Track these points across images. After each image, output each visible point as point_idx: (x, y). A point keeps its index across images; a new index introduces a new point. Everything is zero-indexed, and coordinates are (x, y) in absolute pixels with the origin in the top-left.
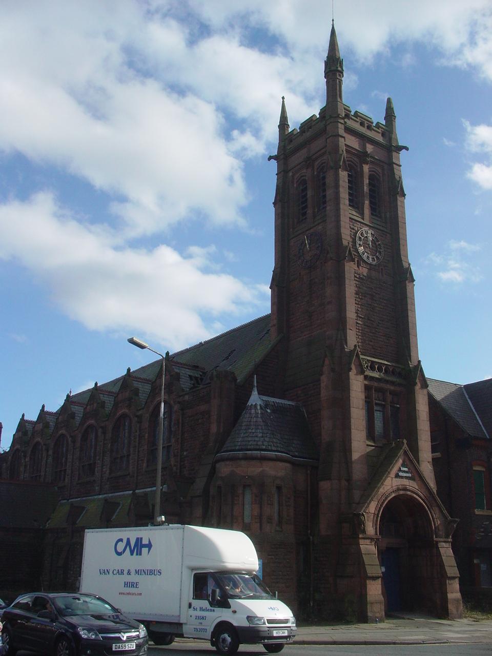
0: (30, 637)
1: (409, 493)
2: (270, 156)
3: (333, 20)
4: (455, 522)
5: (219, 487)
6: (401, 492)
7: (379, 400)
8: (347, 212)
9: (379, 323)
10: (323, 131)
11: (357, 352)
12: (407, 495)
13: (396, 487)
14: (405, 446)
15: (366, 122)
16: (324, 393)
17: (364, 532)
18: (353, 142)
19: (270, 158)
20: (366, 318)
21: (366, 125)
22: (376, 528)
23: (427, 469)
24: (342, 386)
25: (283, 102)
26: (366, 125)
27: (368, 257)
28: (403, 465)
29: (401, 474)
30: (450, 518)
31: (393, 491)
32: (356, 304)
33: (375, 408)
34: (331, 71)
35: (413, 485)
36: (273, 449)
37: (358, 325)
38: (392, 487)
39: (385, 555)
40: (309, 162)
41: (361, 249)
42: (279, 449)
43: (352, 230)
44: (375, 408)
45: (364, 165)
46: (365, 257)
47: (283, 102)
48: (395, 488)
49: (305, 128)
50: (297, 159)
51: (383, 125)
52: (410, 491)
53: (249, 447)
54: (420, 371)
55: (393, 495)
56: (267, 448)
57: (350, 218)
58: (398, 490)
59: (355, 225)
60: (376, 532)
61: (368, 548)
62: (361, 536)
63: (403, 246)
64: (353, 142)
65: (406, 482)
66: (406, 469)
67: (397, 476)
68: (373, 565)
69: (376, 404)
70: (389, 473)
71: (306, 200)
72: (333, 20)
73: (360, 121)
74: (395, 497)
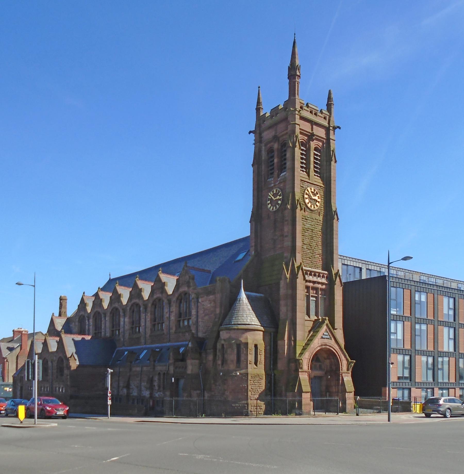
0: (202, 384)
1: (328, 347)
2: (250, 131)
3: (295, 34)
4: (352, 362)
5: (223, 345)
6: (324, 347)
7: (314, 294)
8: (300, 174)
9: (315, 246)
10: (285, 119)
11: (300, 202)
12: (327, 348)
13: (321, 344)
14: (327, 322)
15: (314, 110)
16: (282, 291)
17: (302, 368)
18: (307, 127)
19: (250, 132)
20: (308, 244)
21: (314, 113)
22: (309, 366)
23: (339, 334)
24: (293, 286)
26: (314, 113)
27: (311, 206)
28: (326, 331)
29: (324, 337)
30: (350, 360)
31: (319, 346)
32: (302, 235)
33: (311, 298)
34: (292, 75)
35: (332, 342)
36: (253, 324)
37: (303, 249)
38: (318, 344)
39: (312, 380)
40: (276, 138)
41: (307, 201)
42: (256, 324)
43: (302, 188)
44: (311, 298)
45: (311, 142)
48: (320, 344)
49: (273, 114)
50: (267, 135)
51: (320, 145)
52: (328, 346)
53: (239, 323)
54: (339, 276)
55: (319, 348)
56: (250, 324)
57: (301, 180)
58: (322, 345)
59: (304, 184)
60: (308, 368)
61: (304, 377)
62: (300, 370)
63: (333, 196)
64: (307, 127)
65: (326, 341)
66: (327, 334)
67: (322, 338)
68: (306, 386)
69: (312, 296)
70: (317, 336)
71: (273, 164)
72: (295, 34)
73: (310, 110)
74: (320, 349)
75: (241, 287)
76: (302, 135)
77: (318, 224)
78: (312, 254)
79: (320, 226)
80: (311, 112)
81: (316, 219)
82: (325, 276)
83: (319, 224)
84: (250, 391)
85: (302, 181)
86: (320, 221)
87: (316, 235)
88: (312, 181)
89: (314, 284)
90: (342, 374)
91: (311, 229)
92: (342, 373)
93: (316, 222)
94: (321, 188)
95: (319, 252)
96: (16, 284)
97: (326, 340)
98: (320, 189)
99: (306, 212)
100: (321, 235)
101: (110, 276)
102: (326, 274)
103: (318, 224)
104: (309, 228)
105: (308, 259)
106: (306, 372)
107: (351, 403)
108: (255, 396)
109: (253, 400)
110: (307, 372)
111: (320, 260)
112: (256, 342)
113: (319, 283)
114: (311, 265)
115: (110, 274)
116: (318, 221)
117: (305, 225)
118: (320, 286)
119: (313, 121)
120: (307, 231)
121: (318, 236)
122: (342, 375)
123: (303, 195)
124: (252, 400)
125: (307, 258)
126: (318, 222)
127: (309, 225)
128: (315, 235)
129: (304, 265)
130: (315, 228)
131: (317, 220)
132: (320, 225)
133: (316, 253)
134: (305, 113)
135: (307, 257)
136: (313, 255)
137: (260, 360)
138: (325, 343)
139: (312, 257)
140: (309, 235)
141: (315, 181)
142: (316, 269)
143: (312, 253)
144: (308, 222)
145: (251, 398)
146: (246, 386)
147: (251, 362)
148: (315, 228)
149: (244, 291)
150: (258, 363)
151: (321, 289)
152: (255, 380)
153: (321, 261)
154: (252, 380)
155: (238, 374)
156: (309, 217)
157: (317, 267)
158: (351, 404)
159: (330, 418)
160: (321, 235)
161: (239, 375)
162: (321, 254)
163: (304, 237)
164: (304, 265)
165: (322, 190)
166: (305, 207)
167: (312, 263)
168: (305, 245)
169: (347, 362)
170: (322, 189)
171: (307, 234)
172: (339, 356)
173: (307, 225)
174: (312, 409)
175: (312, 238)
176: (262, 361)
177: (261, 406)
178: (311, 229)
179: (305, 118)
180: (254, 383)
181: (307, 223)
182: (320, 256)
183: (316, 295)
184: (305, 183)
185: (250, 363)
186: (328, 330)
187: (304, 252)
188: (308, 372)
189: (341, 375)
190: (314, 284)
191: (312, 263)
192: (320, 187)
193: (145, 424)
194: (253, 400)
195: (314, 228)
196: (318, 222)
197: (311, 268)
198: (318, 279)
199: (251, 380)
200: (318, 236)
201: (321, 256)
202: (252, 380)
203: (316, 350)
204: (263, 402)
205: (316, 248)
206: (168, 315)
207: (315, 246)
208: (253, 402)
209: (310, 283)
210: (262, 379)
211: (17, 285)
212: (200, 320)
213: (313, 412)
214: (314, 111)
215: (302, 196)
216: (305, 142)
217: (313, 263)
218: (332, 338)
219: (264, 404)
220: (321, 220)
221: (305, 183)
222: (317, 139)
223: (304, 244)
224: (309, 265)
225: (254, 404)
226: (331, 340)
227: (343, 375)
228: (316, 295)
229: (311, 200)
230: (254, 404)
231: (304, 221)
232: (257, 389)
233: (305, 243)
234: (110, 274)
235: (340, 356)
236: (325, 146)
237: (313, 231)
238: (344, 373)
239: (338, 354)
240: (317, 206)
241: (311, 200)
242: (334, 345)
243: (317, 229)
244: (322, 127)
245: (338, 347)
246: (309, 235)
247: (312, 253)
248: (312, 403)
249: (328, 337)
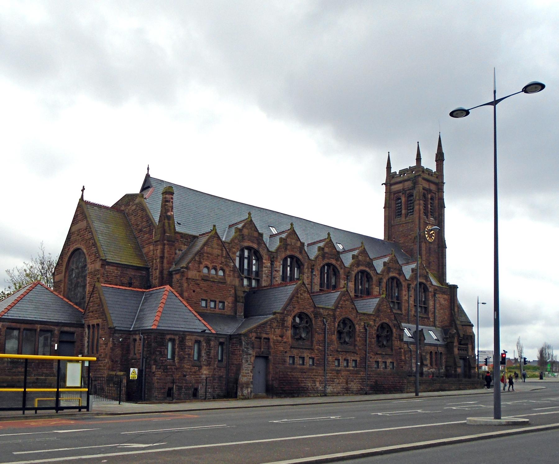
25: (418, 145)
27: (429, 239)
47: (418, 145)
101: (148, 170)
115: (148, 168)
206: (406, 298)
212: (437, 311)
234: (148, 168)
240: (433, 239)
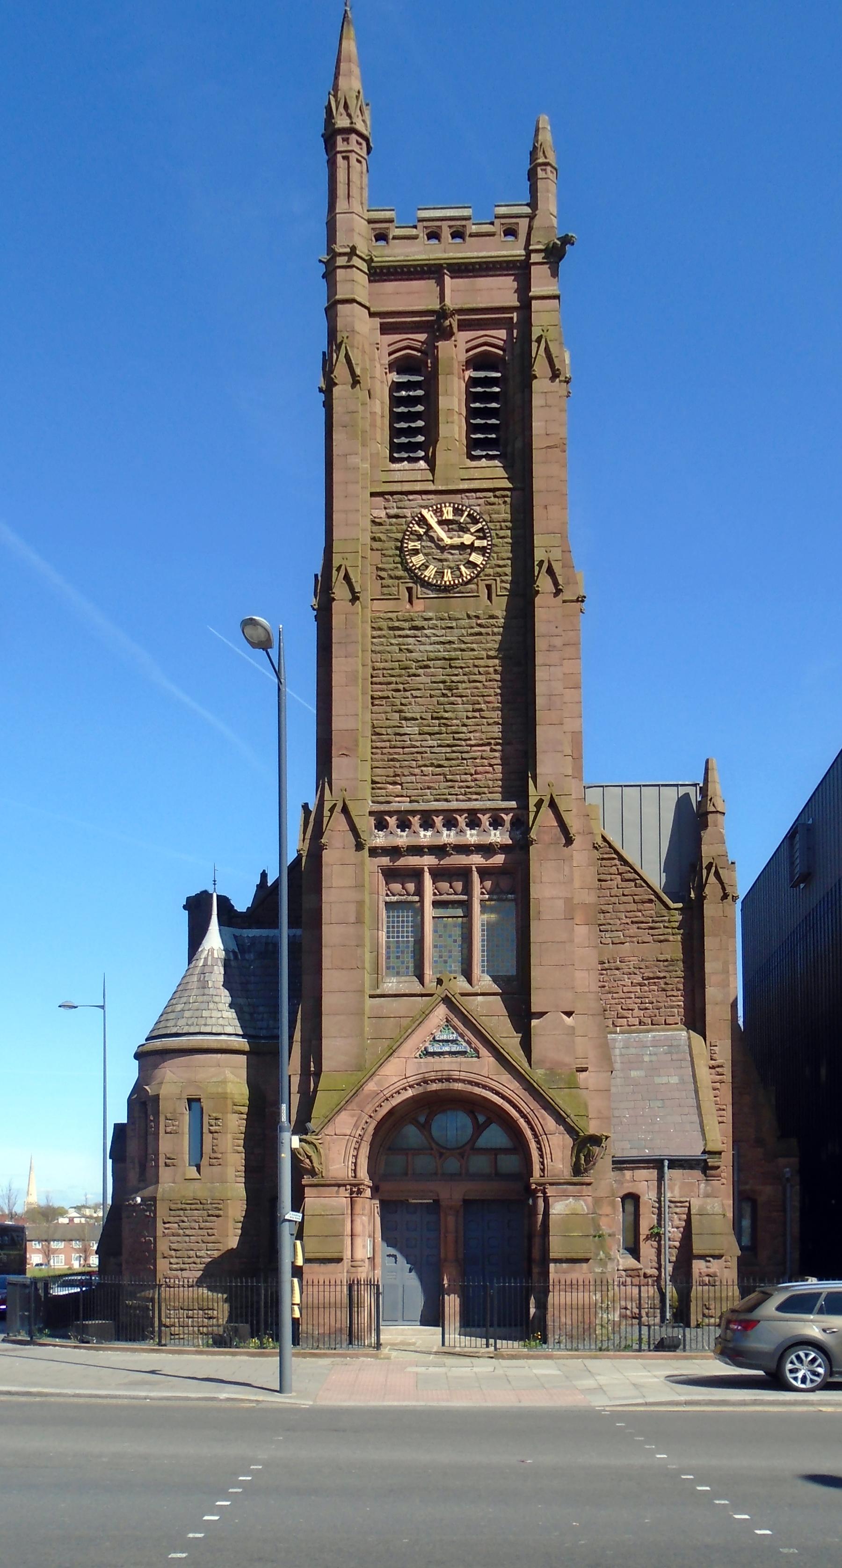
7: (456, 894)
9: (468, 718)
46: (430, 573)
52: (463, 1081)
65: (446, 1064)
66: (454, 1036)
75: (210, 918)
76: (400, 333)
77: (480, 634)
78: (448, 750)
79: (494, 638)
80: (434, 235)
81: (469, 617)
82: (507, 818)
83: (483, 630)
84: (164, 1257)
85: (395, 496)
86: (492, 617)
87: (471, 673)
88: (447, 481)
89: (440, 860)
90: (545, 1188)
91: (445, 659)
92: (545, 1184)
93: (475, 625)
94: (495, 496)
95: (490, 735)
96: (60, 1006)
97: (448, 1059)
98: (493, 500)
99: (415, 601)
100: (496, 671)
102: (506, 811)
103: (480, 634)
104: (432, 655)
105: (430, 769)
106: (339, 1186)
107: (575, 1306)
108: (185, 1274)
109: (179, 1287)
110: (345, 1185)
111: (491, 765)
112: (193, 1092)
113: (464, 849)
114: (446, 791)
116: (479, 622)
117: (410, 651)
118: (477, 859)
119: (441, 265)
120: (421, 671)
121: (482, 678)
122: (544, 1193)
123: (399, 544)
124: (170, 1287)
125: (425, 766)
126: (480, 626)
127: (431, 644)
128: (464, 675)
129: (409, 797)
130: (462, 650)
131: (477, 617)
132: (494, 634)
133: (472, 742)
134: (397, 251)
135: (420, 763)
136: (454, 752)
137: (214, 1151)
138: (440, 1073)
139: (447, 759)
140: (435, 682)
141: (462, 480)
142: (470, 800)
143: (448, 746)
144: (427, 636)
145: (168, 1280)
146: (152, 1239)
147: (169, 1159)
148: (462, 650)
149: (221, 923)
150: (205, 1162)
151: (484, 873)
152: (183, 1222)
153: (499, 768)
154: (172, 1219)
155: (139, 1200)
156: (430, 614)
157: (479, 790)
158: (252, 1307)
159: (164, 1355)
160: (497, 668)
161: (140, 1204)
162: (500, 741)
163: (408, 694)
164: (409, 797)
165: (505, 502)
166: (411, 585)
167: (449, 784)
168: (409, 723)
169: (574, 1140)
170: (504, 496)
171: (423, 679)
172: (524, 1116)
173: (422, 648)
174: (458, 1324)
175: (451, 690)
176: (220, 1156)
177: (211, 1307)
178: (445, 659)
179: (463, 267)
180: (181, 1232)
181: (423, 639)
182: (492, 750)
183: (465, 897)
184: (409, 500)
185: (166, 1165)
186: (455, 1019)
187: (403, 748)
188: (348, 1187)
189: (540, 1194)
190: (440, 860)
191: (447, 781)
192: (491, 494)
193: (26, 1349)
194: (179, 1287)
195: (459, 653)
196: (480, 626)
197: (446, 800)
198: (468, 836)
199: (166, 1221)
200: (482, 678)
201: (499, 747)
202: (172, 1219)
203: (395, 1102)
204: (220, 1295)
205: (469, 722)
207: (468, 718)
208: (172, 1293)
209: (422, 856)
210: (218, 1216)
211: (61, 1008)
213: (460, 1335)
214: (450, 227)
215: (397, 548)
216: (419, 354)
217: (451, 781)
218: (483, 1051)
219: (226, 1301)
220: (500, 613)
221: (409, 500)
222: (464, 326)
223: (406, 719)
224: (435, 792)
225: (181, 1300)
226: (478, 1057)
227: (550, 1191)
228: (465, 897)
229: (442, 552)
230: (181, 1300)
231: (407, 636)
232: (193, 1250)
233: (409, 715)
235: (531, 1116)
236: (515, 335)
237: (454, 663)
238: (551, 1184)
239: (520, 1111)
241: (442, 552)
242: (494, 1077)
243: (476, 653)
244: (504, 269)
245: (515, 1085)
246: (435, 682)
247: (448, 746)
248: (458, 1300)
249: (463, 1046)
